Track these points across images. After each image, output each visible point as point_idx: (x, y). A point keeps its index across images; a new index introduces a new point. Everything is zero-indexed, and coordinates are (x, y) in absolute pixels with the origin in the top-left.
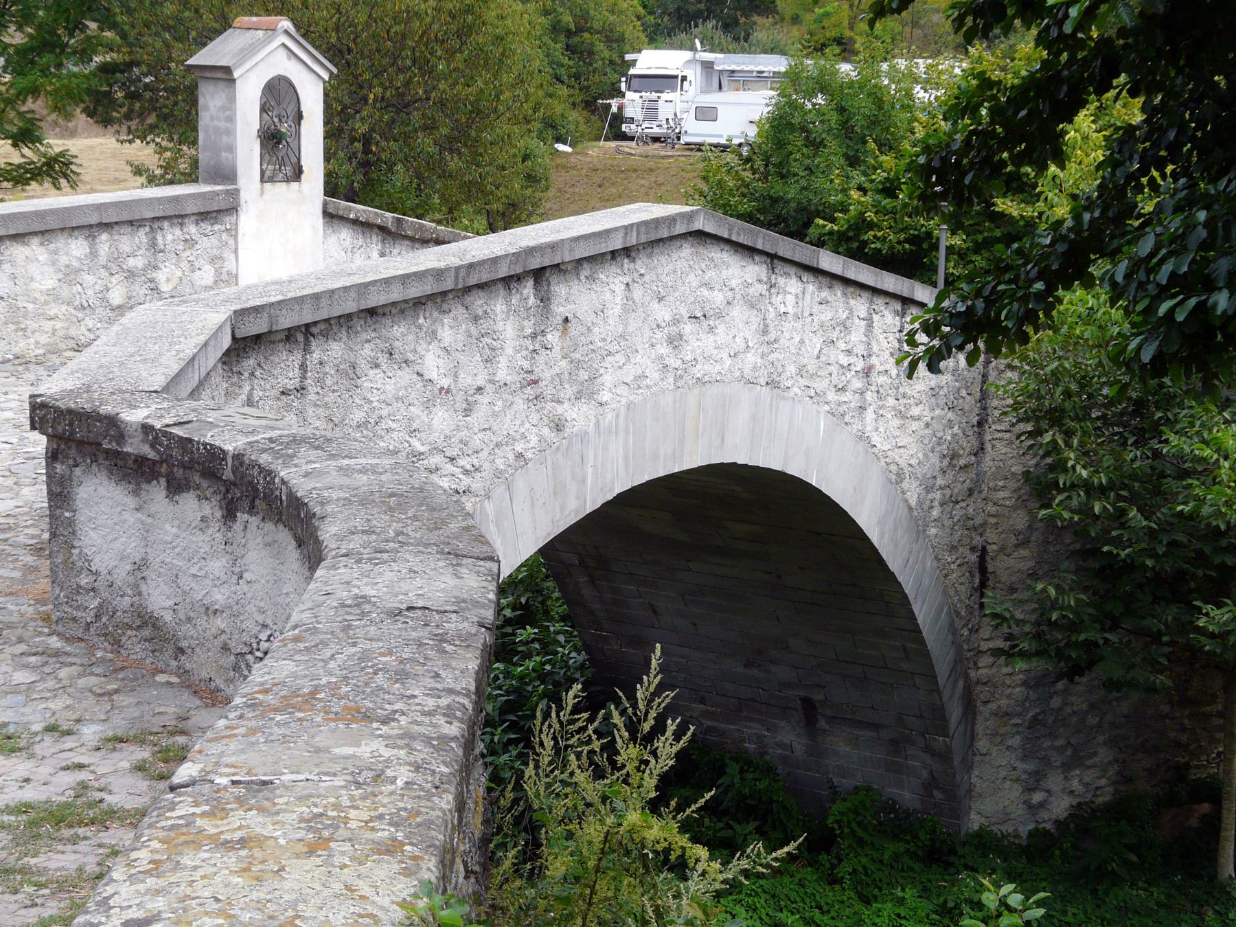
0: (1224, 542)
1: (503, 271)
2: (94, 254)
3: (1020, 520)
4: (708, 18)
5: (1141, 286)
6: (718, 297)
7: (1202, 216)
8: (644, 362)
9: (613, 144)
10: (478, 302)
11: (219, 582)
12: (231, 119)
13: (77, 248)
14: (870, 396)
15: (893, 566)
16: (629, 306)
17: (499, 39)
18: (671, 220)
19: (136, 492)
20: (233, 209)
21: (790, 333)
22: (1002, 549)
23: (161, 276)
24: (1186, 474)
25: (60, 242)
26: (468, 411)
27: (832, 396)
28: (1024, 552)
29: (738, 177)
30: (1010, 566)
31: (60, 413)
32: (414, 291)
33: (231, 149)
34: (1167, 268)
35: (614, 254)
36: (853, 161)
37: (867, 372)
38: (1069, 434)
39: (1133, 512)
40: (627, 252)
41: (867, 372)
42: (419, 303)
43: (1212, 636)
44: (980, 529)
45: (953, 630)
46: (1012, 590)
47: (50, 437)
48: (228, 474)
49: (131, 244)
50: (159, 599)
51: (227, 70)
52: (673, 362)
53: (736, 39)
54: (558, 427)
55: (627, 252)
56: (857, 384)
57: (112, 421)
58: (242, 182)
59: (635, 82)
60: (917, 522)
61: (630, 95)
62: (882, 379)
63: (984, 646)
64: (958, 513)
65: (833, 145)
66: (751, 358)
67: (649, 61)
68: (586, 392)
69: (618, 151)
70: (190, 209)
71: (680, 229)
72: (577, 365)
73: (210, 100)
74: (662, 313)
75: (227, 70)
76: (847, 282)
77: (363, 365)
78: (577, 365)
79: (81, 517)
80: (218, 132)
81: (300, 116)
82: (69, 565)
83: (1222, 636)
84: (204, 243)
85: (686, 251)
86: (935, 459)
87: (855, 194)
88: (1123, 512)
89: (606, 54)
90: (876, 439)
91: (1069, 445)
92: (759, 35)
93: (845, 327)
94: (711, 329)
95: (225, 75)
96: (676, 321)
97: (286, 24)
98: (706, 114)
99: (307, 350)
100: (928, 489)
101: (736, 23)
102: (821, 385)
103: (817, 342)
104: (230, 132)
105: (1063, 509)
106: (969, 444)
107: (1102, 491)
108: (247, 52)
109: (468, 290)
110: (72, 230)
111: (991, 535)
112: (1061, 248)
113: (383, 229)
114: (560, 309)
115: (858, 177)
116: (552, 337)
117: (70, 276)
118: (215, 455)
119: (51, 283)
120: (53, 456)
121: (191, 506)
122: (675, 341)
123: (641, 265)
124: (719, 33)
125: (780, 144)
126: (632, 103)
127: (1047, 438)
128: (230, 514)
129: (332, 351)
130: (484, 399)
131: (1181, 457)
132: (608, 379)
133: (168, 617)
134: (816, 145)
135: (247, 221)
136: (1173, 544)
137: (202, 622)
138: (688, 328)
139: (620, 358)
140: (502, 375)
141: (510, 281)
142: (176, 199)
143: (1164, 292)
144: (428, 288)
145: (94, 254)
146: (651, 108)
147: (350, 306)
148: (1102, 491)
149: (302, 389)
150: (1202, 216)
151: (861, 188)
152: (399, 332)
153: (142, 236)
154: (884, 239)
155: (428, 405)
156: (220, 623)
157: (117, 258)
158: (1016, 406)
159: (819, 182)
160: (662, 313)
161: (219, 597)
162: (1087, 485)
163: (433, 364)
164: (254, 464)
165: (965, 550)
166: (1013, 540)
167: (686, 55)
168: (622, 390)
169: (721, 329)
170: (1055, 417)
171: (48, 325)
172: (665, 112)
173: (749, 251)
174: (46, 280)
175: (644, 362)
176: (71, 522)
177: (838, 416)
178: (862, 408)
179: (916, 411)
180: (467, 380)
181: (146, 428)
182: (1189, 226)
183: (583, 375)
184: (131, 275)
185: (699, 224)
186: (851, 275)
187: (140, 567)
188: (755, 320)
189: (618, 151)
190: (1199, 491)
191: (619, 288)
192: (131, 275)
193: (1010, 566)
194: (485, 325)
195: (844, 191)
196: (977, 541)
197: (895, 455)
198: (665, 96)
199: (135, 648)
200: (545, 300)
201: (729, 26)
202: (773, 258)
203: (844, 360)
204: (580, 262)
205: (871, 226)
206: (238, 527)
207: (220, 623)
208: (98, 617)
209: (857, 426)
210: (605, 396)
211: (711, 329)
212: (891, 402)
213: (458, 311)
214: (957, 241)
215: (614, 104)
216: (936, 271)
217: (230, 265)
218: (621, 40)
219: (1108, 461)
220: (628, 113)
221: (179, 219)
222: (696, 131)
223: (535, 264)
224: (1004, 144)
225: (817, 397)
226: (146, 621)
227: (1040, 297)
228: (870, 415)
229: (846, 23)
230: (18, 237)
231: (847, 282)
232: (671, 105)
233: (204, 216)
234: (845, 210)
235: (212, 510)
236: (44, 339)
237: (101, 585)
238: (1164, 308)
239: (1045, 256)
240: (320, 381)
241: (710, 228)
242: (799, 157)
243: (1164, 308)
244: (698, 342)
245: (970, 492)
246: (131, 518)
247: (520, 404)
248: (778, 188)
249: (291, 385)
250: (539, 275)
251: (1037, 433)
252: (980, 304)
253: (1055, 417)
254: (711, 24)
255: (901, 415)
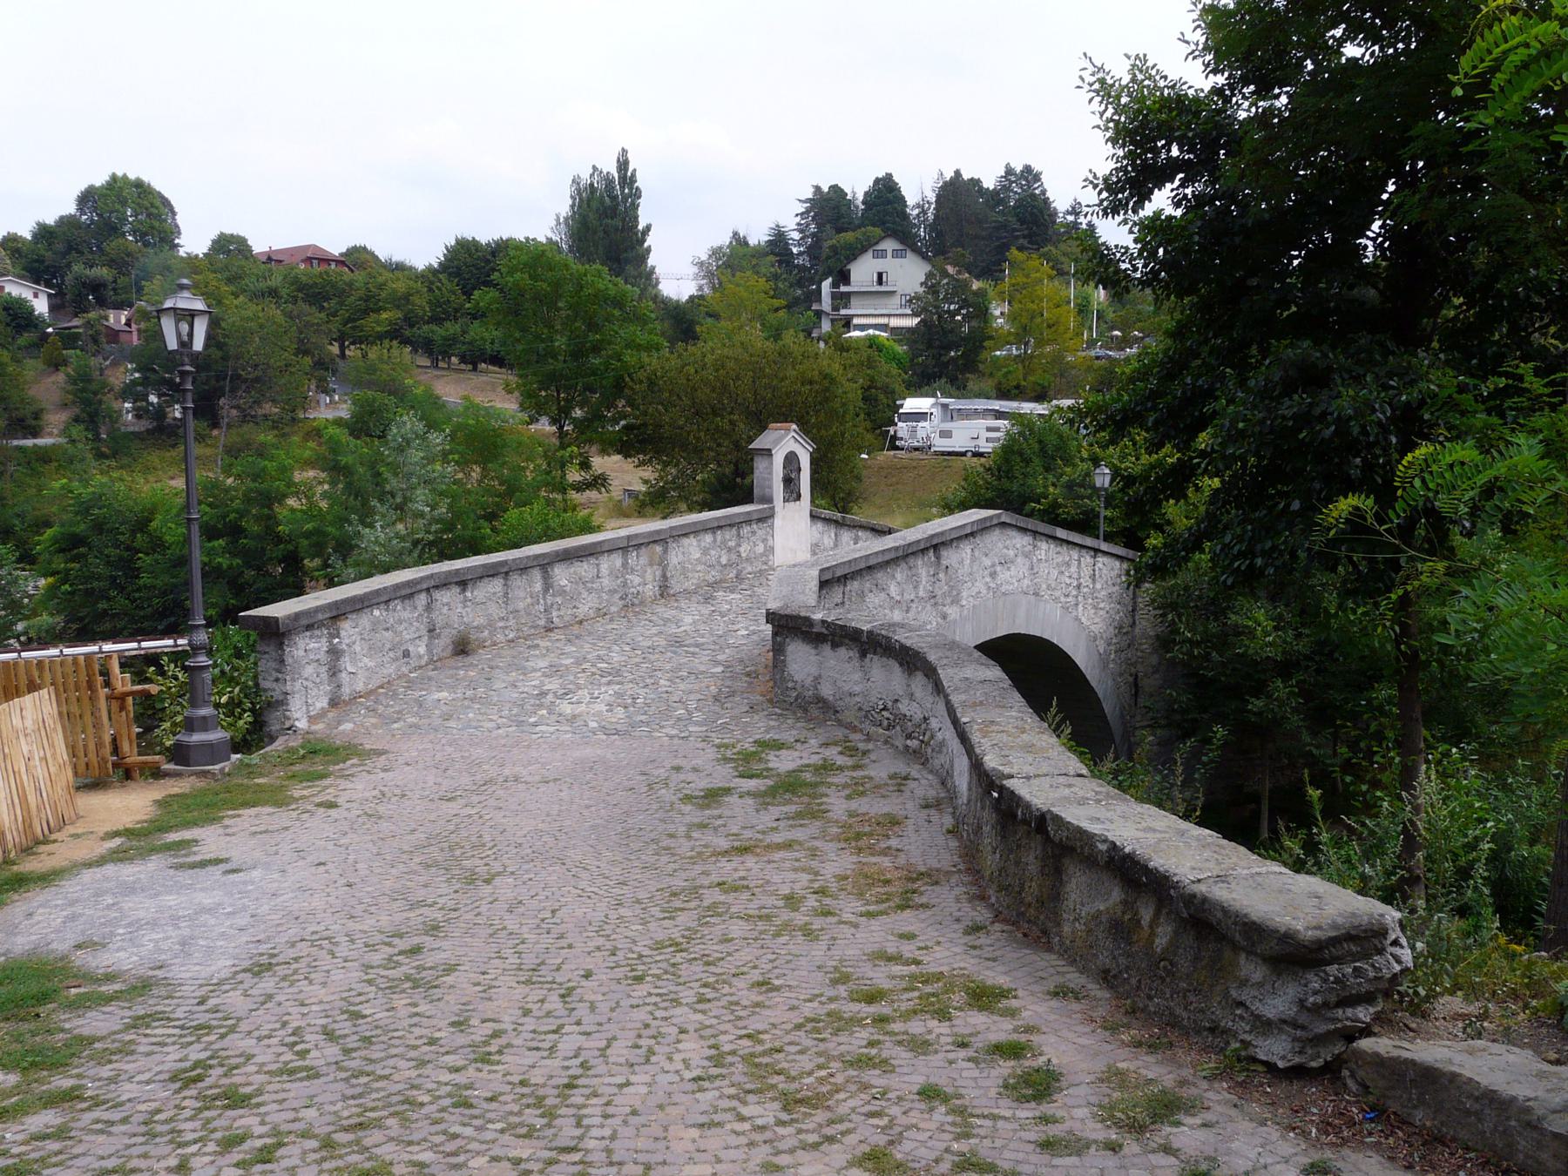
0: (1259, 668)
1: (922, 546)
2: (715, 541)
3: (1154, 660)
4: (940, 377)
5: (1227, 555)
6: (1011, 553)
7: (1249, 527)
8: (980, 585)
9: (892, 453)
10: (911, 561)
11: (856, 683)
12: (771, 473)
13: (708, 538)
14: (1080, 599)
15: (1094, 684)
16: (973, 559)
17: (844, 404)
18: (991, 518)
19: (816, 648)
20: (772, 516)
21: (1043, 569)
22: (1145, 675)
23: (742, 549)
24: (1240, 634)
25: (701, 536)
26: (907, 611)
27: (1063, 599)
28: (1157, 676)
29: (983, 478)
30: (1149, 684)
31: (782, 616)
32: (888, 557)
33: (770, 487)
34: (1237, 548)
35: (967, 536)
36: (1047, 469)
37: (1079, 587)
38: (1180, 616)
39: (1214, 654)
40: (972, 534)
41: (1079, 587)
42: (888, 563)
43: (1255, 714)
44: (1134, 665)
45: (1122, 716)
46: (1151, 695)
47: (774, 626)
48: (864, 639)
49: (729, 534)
50: (826, 691)
51: (770, 450)
52: (993, 585)
53: (958, 388)
54: (944, 617)
55: (972, 534)
56: (1074, 593)
57: (807, 619)
58: (775, 502)
59: (903, 417)
60: (1104, 662)
61: (900, 424)
62: (1085, 590)
63: (1138, 725)
64: (1123, 656)
65: (1036, 461)
66: (1026, 582)
67: (911, 404)
68: (956, 601)
69: (895, 457)
70: (755, 516)
71: (995, 521)
72: (952, 588)
73: (760, 465)
74: (987, 562)
75: (770, 450)
76: (1068, 542)
77: (866, 591)
78: (952, 588)
79: (788, 659)
80: (764, 479)
81: (800, 470)
82: (783, 680)
83: (1260, 714)
84: (760, 533)
85: (997, 532)
86: (1111, 629)
87: (1051, 489)
88: (1209, 654)
89: (885, 401)
90: (1083, 620)
91: (1180, 621)
92: (970, 385)
93: (1068, 565)
94: (1009, 569)
95: (768, 453)
96: (993, 566)
97: (794, 426)
98: (946, 434)
99: (845, 585)
100: (1109, 645)
101: (957, 379)
102: (1058, 593)
103: (1056, 573)
104: (771, 480)
105: (1177, 653)
106: (1128, 621)
107: (1198, 644)
108: (778, 441)
109: (907, 555)
110: (706, 530)
111: (1140, 667)
112: (1192, 538)
113: (836, 522)
114: (944, 562)
115: (1051, 478)
116: (941, 575)
117: (705, 552)
118: (858, 632)
119: (698, 555)
120: (775, 634)
121: (843, 652)
122: (993, 575)
123: (978, 540)
124: (949, 386)
125: (1007, 461)
126: (902, 428)
127: (1170, 617)
128: (863, 655)
129: (854, 586)
130: (914, 605)
131: (1236, 625)
132: (964, 594)
133: (831, 698)
134: (1028, 461)
135: (778, 521)
136: (1234, 669)
137: (847, 699)
138: (998, 568)
139: (969, 584)
140: (921, 594)
141: (924, 551)
142: (748, 513)
143: (1236, 558)
144: (892, 555)
145: (715, 541)
146: (914, 431)
147: (863, 565)
148: (1198, 644)
149: (843, 603)
150: (1249, 527)
151: (1054, 485)
152: (880, 576)
153: (734, 531)
154: (1068, 513)
155: (892, 609)
156: (858, 699)
157: (724, 542)
158: (1153, 601)
159: (1030, 481)
160: (987, 562)
161: (857, 689)
162: (1190, 641)
163: (893, 590)
164: (879, 635)
165: (1126, 675)
166: (1151, 670)
167: (931, 401)
168: (971, 599)
169: (1013, 568)
170: (1173, 606)
171: (696, 575)
172: (921, 434)
173: (1023, 530)
174: (696, 554)
175: (980, 585)
176: (784, 661)
177: (1065, 608)
178: (1077, 605)
179: (1102, 605)
180: (907, 597)
181: (823, 622)
182: (1244, 531)
183: (955, 593)
184: (730, 550)
185: (1004, 519)
186: (1071, 539)
187: (817, 679)
188: (1028, 563)
189: (895, 457)
190: (1247, 642)
191: (969, 551)
192: (730, 550)
193: (1149, 684)
194: (914, 571)
195: (1045, 487)
196: (1133, 670)
197: (1092, 628)
198: (920, 424)
199: (814, 711)
200: (938, 558)
201: (953, 380)
202: (1035, 533)
203: (1068, 581)
204: (952, 540)
205: (1060, 506)
206: (867, 660)
207: (858, 699)
208: (796, 700)
209: (1075, 613)
210: (964, 603)
211: (1009, 569)
212: (1090, 601)
213: (904, 565)
214: (1108, 513)
215: (892, 430)
216: (1098, 528)
217: (770, 543)
218: (893, 392)
219: (1201, 629)
220: (900, 434)
221: (749, 522)
222: (941, 444)
223: (935, 542)
224: (1163, 491)
225: (1056, 600)
226: (820, 701)
227: (1183, 558)
228: (1080, 608)
229: (1021, 377)
230: (686, 535)
231: (1068, 542)
232: (924, 428)
233: (760, 520)
234: (1046, 498)
235: (854, 654)
236: (695, 581)
237: (798, 686)
238: (1236, 564)
239: (1185, 540)
240: (850, 599)
241: (1008, 521)
242: (1018, 470)
243: (1236, 564)
244: (1003, 575)
245: (1129, 646)
246: (813, 658)
247: (929, 607)
248: (1006, 484)
249: (839, 601)
250: (936, 547)
251: (1164, 615)
252: (1158, 561)
253: (1173, 606)
254: (943, 380)
255: (1095, 607)
